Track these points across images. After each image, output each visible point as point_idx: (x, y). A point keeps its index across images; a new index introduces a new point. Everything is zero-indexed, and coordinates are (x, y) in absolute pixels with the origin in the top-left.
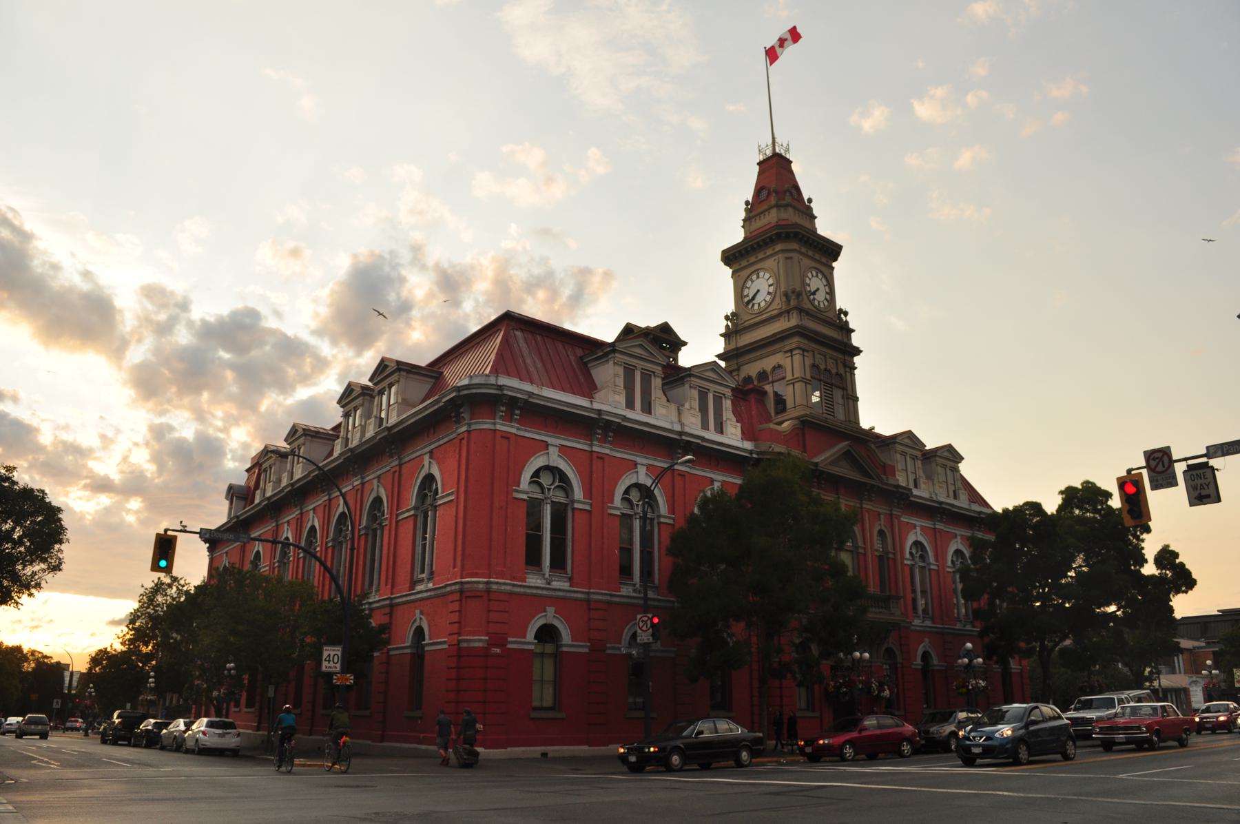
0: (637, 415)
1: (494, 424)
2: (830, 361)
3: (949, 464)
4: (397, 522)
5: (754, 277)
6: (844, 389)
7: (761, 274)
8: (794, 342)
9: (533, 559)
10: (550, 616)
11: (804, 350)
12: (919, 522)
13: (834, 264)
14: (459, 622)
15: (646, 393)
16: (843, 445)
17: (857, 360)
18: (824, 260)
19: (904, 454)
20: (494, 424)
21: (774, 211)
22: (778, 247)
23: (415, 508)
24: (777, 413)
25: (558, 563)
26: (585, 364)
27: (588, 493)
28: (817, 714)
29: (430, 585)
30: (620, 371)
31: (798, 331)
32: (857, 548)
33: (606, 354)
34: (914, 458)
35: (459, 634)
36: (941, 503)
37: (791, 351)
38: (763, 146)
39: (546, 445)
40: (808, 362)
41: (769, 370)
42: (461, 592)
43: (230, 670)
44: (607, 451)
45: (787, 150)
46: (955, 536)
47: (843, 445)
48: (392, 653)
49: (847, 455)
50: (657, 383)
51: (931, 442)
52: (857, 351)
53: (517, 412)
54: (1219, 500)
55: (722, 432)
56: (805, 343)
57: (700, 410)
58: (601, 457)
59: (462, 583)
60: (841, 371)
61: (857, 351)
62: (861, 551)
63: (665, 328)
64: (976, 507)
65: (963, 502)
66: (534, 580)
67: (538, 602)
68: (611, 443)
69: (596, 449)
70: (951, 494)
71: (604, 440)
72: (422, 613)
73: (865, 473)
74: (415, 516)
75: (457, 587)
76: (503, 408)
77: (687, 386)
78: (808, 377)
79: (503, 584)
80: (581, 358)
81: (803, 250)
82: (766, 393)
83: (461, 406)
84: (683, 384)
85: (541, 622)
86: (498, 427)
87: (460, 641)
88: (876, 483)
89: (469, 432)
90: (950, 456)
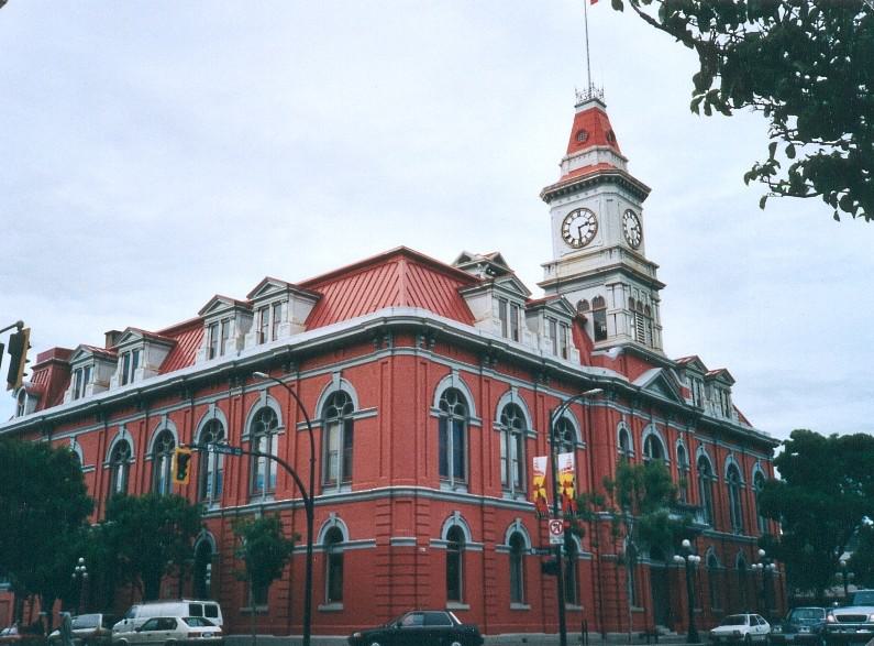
0: (559, 359)
1: (415, 351)
2: (641, 294)
3: (725, 387)
4: (297, 432)
5: (575, 215)
6: (651, 319)
7: (582, 213)
8: (618, 278)
9: (444, 470)
10: (456, 520)
11: (624, 285)
12: (733, 448)
13: (643, 205)
14: (391, 524)
15: (515, 323)
16: (655, 372)
17: (661, 293)
18: (635, 202)
19: (691, 378)
20: (415, 351)
21: (595, 154)
22: (601, 189)
23: (322, 421)
24: (597, 339)
25: (460, 473)
26: (461, 295)
27: (480, 413)
28: (642, 609)
29: (347, 490)
30: (496, 303)
31: (622, 269)
32: (685, 466)
33: (485, 289)
34: (698, 381)
35: (391, 535)
36: (544, 360)
37: (613, 285)
38: (580, 90)
39: (451, 370)
40: (627, 295)
41: (590, 300)
42: (392, 497)
43: (81, 572)
44: (492, 375)
45: (602, 95)
46: (730, 452)
47: (655, 372)
48: (393, 545)
49: (659, 381)
50: (522, 313)
51: (712, 365)
52: (662, 286)
53: (433, 341)
54: (649, 190)
55: (516, 339)
56: (625, 280)
57: (501, 318)
58: (542, 396)
59: (392, 490)
60: (649, 303)
61: (662, 286)
62: (632, 455)
63: (725, 373)
64: (744, 426)
65: (734, 421)
66: (445, 488)
67: (450, 503)
68: (433, 349)
69: (484, 373)
70: (559, 351)
71: (490, 366)
72: (337, 515)
73: (670, 395)
74: (322, 428)
75: (388, 493)
76: (423, 338)
77: (541, 316)
78: (627, 309)
79: (424, 489)
80: (457, 290)
81: (621, 193)
82: (586, 320)
83: (384, 335)
84: (537, 315)
85: (452, 524)
86: (419, 354)
87: (391, 542)
88: (680, 404)
89: (393, 357)
90: (724, 380)
